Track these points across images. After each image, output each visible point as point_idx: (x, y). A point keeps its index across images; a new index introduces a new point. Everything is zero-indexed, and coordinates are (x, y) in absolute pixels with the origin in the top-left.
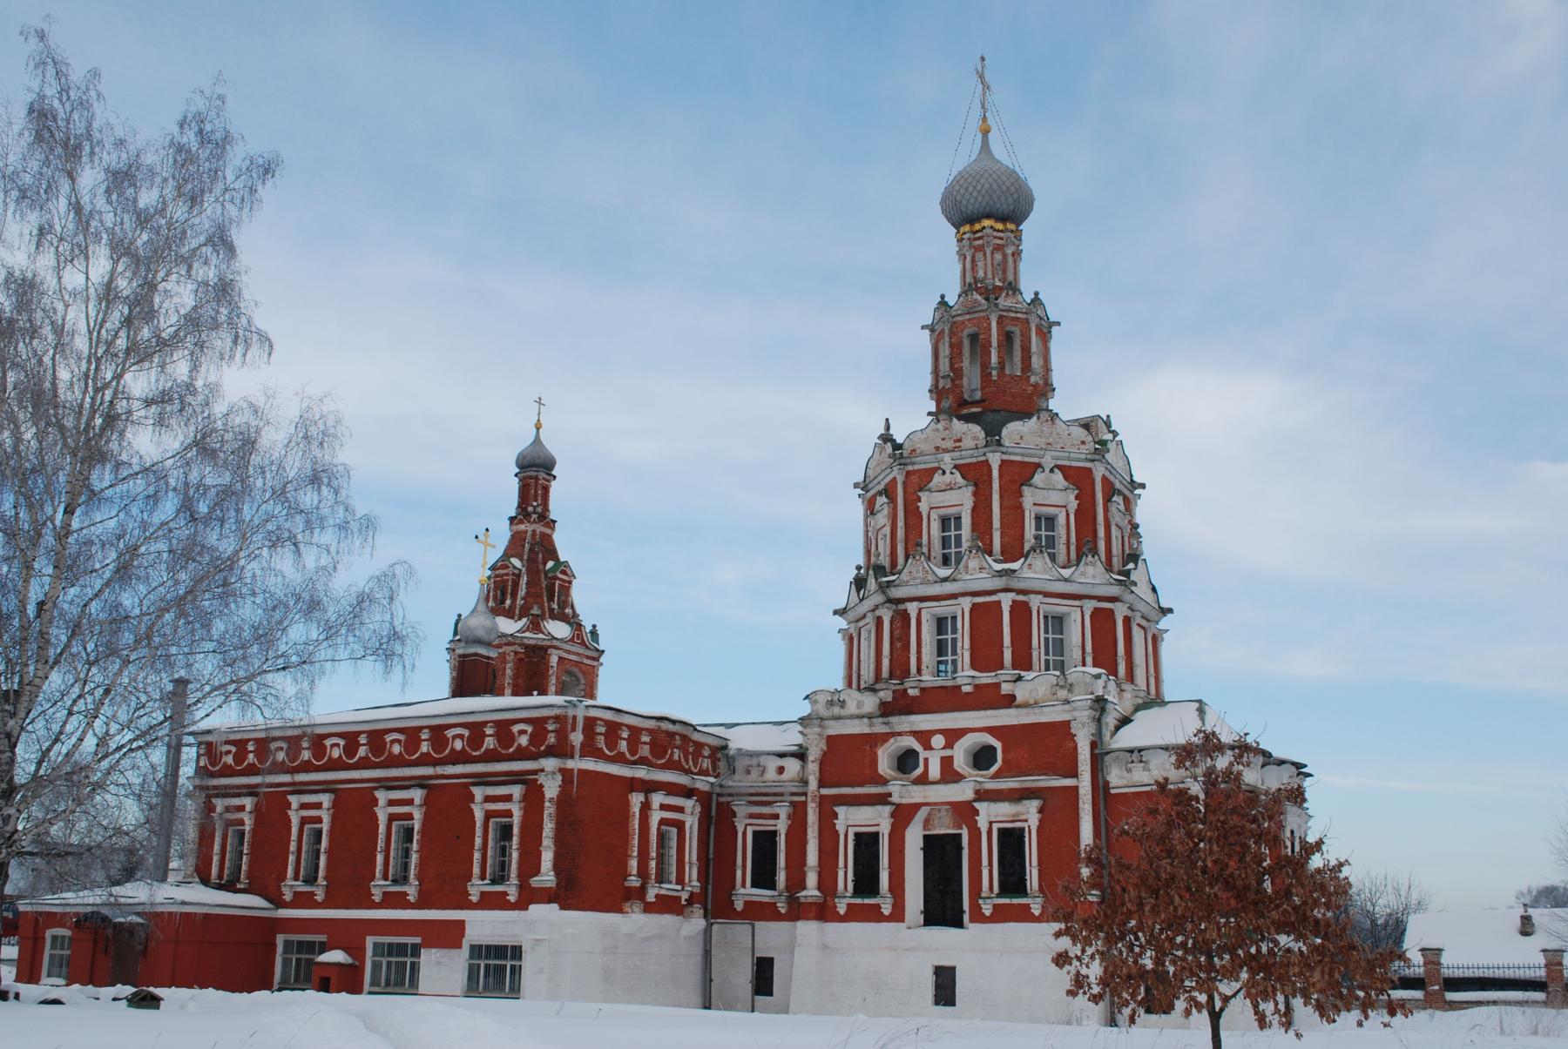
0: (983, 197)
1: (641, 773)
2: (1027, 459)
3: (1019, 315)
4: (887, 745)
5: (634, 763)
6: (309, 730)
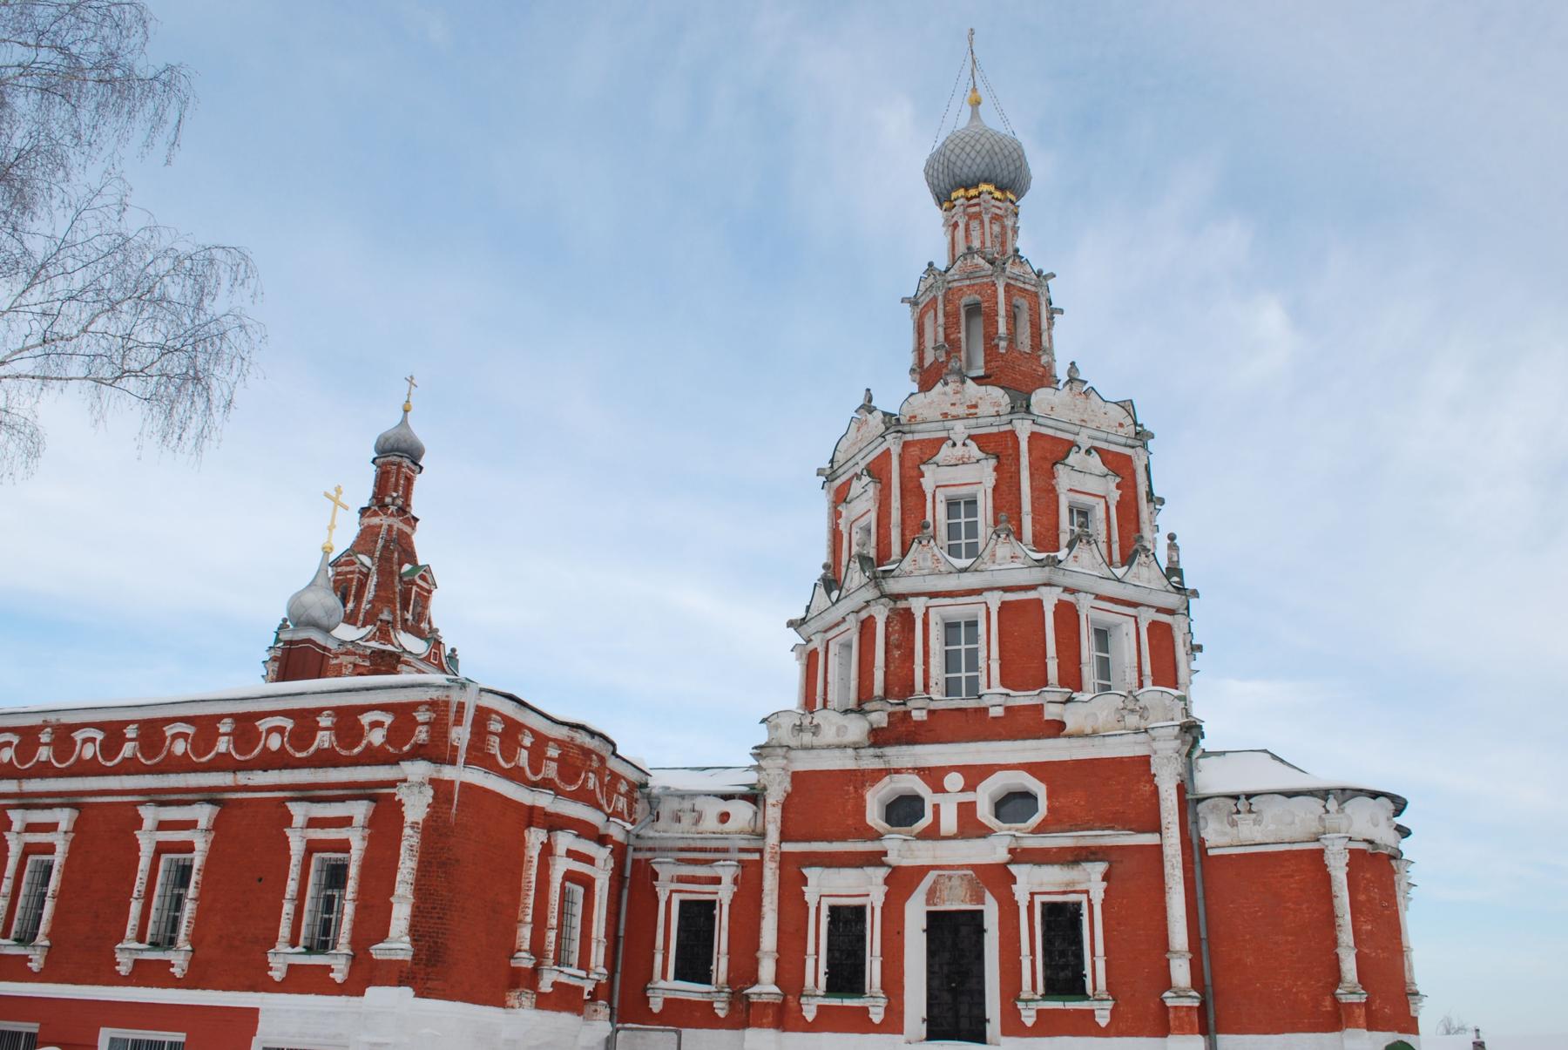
0: (983, 158)
1: (544, 800)
2: (1060, 435)
3: (1028, 287)
4: (879, 785)
5: (535, 785)
6: (52, 718)
